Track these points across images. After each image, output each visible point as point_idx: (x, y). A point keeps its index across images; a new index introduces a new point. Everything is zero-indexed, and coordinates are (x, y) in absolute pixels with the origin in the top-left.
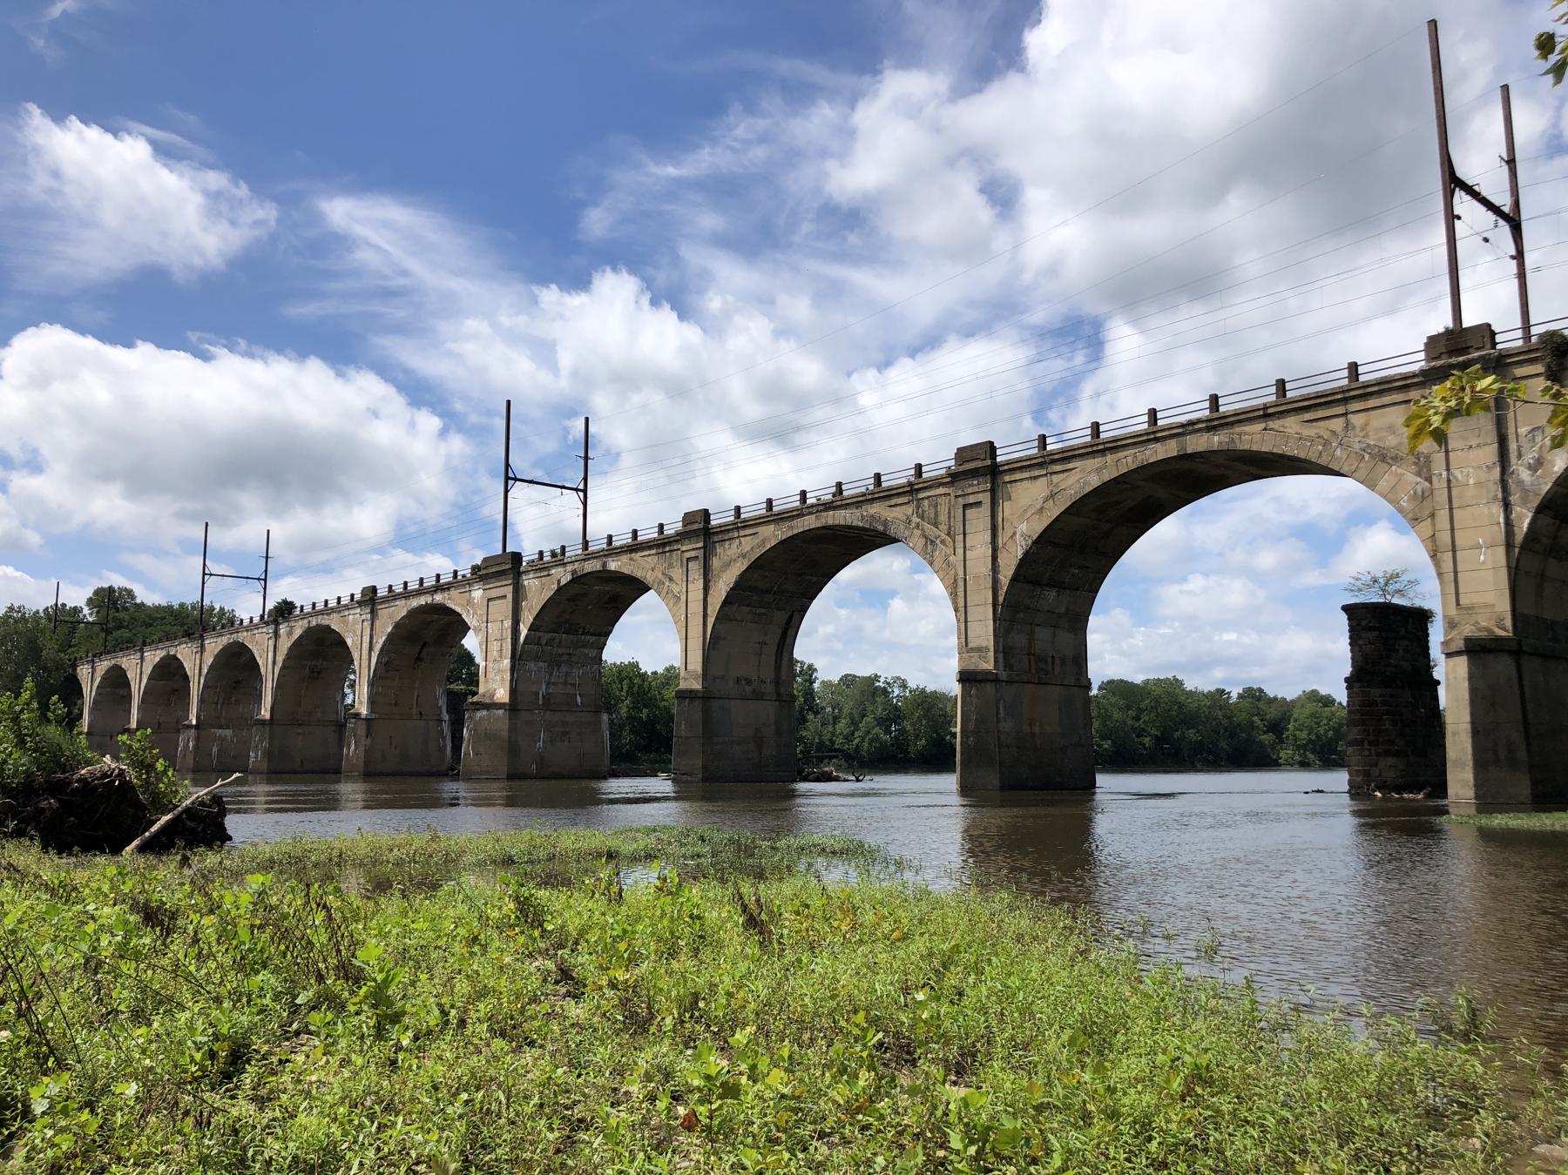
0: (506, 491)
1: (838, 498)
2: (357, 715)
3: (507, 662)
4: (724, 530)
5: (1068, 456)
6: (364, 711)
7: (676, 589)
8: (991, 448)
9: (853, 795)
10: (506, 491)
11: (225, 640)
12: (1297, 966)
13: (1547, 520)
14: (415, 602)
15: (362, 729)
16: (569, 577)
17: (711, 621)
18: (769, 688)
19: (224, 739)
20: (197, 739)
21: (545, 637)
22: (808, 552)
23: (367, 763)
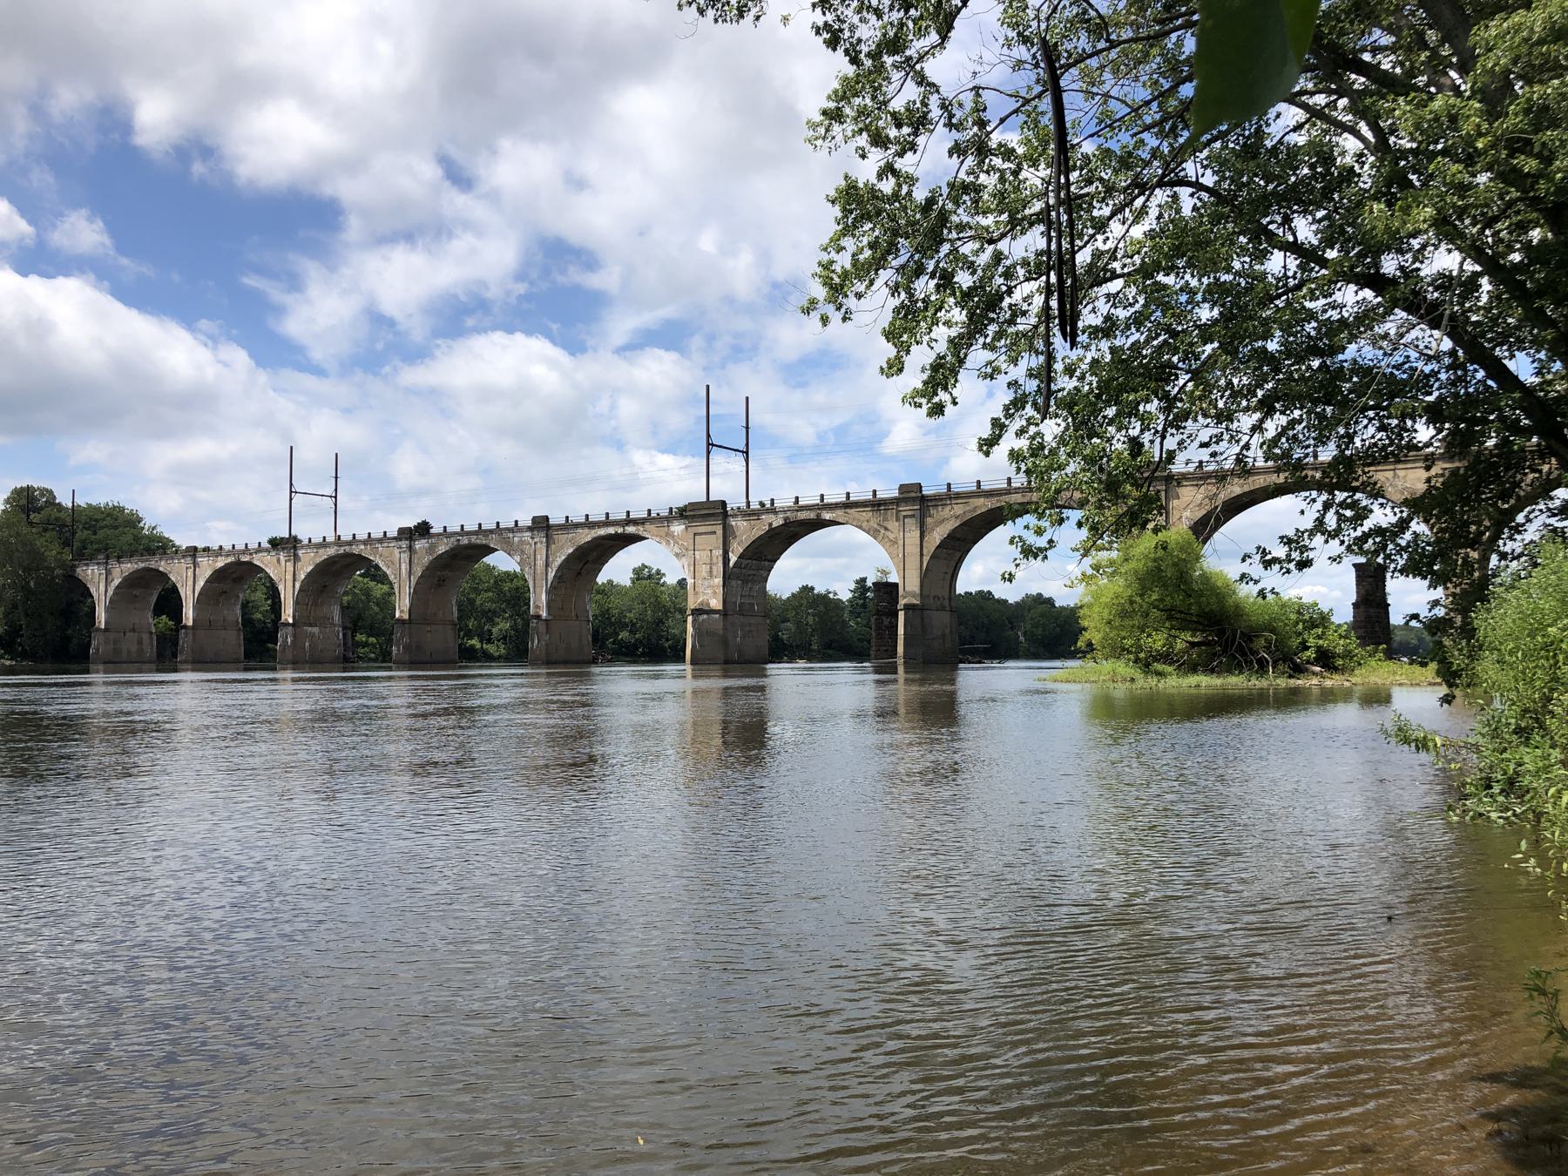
1: (480, 531)
2: (538, 617)
3: (719, 581)
4: (561, 527)
5: (577, 525)
6: (544, 614)
8: (547, 518)
9: (240, 681)
11: (129, 567)
12: (377, 750)
14: (602, 532)
15: (542, 628)
17: (926, 559)
18: (946, 603)
19: (312, 635)
20: (294, 636)
21: (745, 562)
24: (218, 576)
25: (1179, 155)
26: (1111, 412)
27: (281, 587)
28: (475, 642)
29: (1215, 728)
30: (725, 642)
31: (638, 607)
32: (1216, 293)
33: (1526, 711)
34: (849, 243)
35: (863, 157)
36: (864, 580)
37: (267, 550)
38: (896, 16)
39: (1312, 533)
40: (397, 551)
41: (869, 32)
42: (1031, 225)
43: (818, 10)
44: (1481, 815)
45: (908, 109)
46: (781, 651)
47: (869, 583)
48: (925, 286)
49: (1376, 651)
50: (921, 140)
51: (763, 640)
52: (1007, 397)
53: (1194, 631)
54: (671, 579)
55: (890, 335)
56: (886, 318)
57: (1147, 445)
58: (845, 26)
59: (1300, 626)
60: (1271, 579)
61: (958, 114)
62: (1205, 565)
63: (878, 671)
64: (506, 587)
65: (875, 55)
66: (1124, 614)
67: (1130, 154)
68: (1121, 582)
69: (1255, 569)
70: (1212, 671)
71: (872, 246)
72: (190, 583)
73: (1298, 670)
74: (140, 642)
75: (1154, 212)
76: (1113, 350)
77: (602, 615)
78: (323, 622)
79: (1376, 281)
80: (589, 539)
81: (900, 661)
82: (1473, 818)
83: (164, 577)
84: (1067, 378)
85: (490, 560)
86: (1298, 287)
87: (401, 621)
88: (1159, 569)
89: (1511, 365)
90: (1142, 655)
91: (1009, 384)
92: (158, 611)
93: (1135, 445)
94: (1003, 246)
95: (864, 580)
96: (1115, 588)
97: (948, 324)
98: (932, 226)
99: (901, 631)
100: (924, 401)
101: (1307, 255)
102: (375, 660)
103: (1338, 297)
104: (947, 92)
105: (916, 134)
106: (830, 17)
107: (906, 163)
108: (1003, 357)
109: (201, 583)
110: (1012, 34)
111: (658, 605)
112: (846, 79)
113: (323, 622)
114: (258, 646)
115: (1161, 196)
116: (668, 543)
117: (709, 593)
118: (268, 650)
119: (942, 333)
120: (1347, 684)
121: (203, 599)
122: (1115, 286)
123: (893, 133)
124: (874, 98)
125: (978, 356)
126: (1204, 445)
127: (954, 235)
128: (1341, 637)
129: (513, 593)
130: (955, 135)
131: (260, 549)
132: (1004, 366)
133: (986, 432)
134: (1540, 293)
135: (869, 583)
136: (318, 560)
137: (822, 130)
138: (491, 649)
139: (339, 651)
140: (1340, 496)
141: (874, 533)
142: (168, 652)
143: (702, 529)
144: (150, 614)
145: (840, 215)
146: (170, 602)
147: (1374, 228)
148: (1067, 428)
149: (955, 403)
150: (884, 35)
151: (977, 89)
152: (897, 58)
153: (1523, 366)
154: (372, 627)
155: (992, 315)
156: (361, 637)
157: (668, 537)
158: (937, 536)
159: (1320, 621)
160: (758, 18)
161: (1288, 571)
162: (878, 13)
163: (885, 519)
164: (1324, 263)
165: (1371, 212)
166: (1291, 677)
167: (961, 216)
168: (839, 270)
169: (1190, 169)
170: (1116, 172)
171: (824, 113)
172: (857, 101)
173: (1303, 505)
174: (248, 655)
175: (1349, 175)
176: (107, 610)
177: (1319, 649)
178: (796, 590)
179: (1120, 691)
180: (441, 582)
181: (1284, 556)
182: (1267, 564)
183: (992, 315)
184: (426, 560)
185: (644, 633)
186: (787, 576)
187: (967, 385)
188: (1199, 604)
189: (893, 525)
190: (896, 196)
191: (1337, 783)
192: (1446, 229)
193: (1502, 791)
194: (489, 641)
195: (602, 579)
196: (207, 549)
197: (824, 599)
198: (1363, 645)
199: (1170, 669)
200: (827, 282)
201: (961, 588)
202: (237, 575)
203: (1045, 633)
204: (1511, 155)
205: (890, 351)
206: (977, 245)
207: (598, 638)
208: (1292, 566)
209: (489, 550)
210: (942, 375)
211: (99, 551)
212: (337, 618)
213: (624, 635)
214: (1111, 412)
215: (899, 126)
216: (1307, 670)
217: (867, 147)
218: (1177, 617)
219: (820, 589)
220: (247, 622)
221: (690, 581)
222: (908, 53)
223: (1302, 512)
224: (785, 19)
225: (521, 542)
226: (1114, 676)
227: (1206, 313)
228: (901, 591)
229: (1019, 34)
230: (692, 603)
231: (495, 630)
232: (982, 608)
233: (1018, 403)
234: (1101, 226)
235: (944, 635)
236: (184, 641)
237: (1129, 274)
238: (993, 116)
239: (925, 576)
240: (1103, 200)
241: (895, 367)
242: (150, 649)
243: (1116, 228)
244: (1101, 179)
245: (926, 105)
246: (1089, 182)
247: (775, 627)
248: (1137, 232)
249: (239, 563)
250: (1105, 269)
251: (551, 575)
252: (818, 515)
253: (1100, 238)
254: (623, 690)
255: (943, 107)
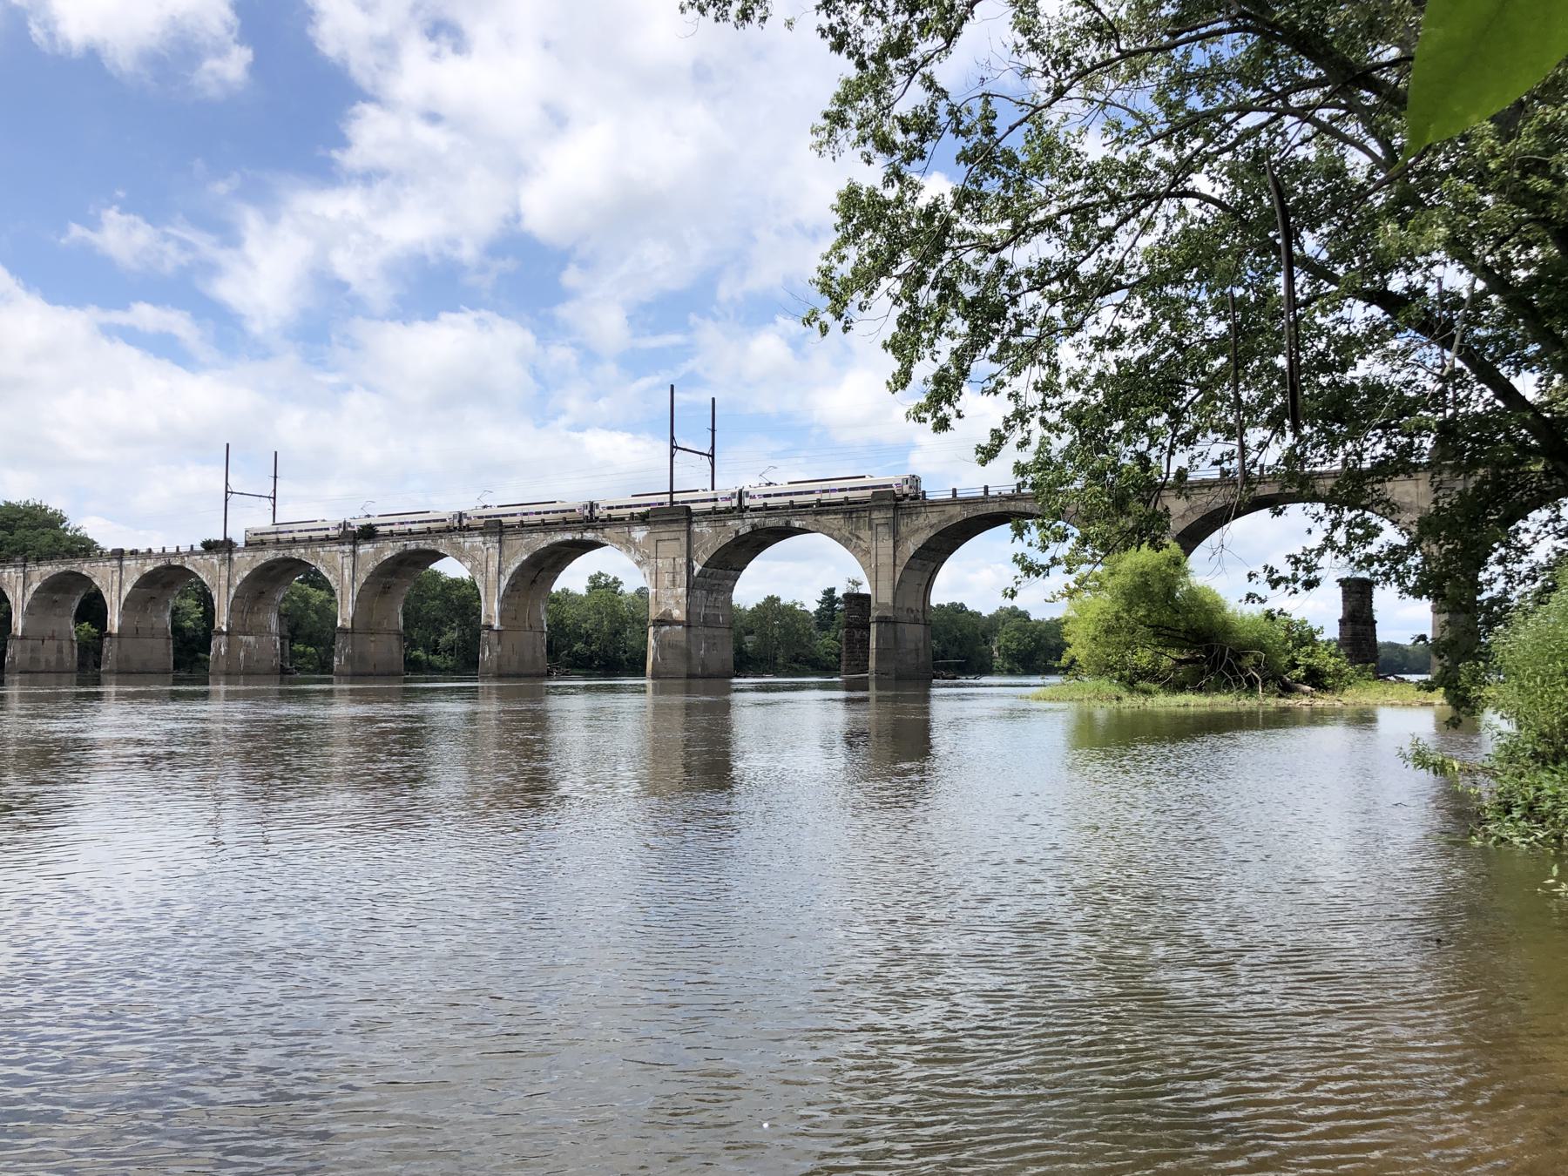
0: (672, 456)
2: (490, 627)
3: (682, 590)
6: (496, 624)
7: (864, 545)
10: (672, 456)
13: (92, 590)
15: (494, 637)
16: (748, 529)
17: (900, 569)
18: (920, 616)
19: (248, 645)
20: (228, 645)
21: (710, 571)
22: (582, 529)
23: (499, 666)
24: (147, 580)
25: (1189, 166)
26: (1118, 426)
27: (214, 593)
28: (420, 653)
29: (1198, 751)
30: (688, 656)
31: (594, 618)
32: (1224, 307)
33: (1542, 735)
34: (852, 252)
35: (869, 162)
36: (832, 590)
37: (199, 553)
38: (902, 18)
39: (1320, 552)
40: (339, 556)
41: (873, 36)
42: (1036, 232)
43: (823, 13)
44: (1503, 840)
45: (915, 115)
46: (746, 663)
47: (839, 594)
48: (927, 296)
49: (1365, 670)
50: (928, 146)
51: (727, 654)
52: (1009, 408)
53: (1181, 648)
54: (629, 587)
55: (895, 346)
56: (891, 328)
57: (1154, 460)
58: (850, 29)
59: (1290, 644)
60: (1279, 600)
61: (967, 121)
62: (1192, 579)
63: (849, 687)
64: (455, 594)
65: (879, 59)
66: (1109, 631)
67: (1136, 165)
68: (1106, 596)
69: (1263, 589)
70: (1200, 689)
71: (872, 255)
72: (115, 589)
73: (1287, 690)
74: (60, 650)
75: (1161, 225)
76: (1119, 364)
77: (556, 626)
78: (261, 631)
79: (1380, 297)
80: (544, 545)
81: (871, 674)
82: (1496, 843)
83: (87, 581)
84: (1073, 391)
85: (436, 566)
86: (1307, 303)
87: (343, 630)
88: (1146, 583)
89: (1516, 382)
90: (1127, 673)
91: (1010, 395)
92: (80, 617)
93: (1142, 459)
94: (1006, 254)
95: (832, 590)
96: (1100, 603)
97: (952, 335)
98: (934, 234)
99: (873, 644)
100: (928, 416)
101: (1318, 271)
102: (314, 672)
103: (1346, 313)
104: (956, 99)
105: (922, 140)
106: (835, 19)
107: (912, 171)
108: (1006, 371)
109: (128, 588)
110: (1022, 40)
111: (614, 615)
112: (848, 82)
113: (261, 631)
114: (188, 659)
115: (1170, 207)
116: (629, 551)
117: (673, 602)
118: (198, 660)
119: (945, 346)
120: (1338, 704)
121: (130, 604)
122: (1119, 296)
123: (899, 137)
124: (877, 102)
125: (982, 366)
126: (1215, 463)
127: (956, 243)
128: (1331, 655)
129: (462, 600)
130: (961, 140)
131: (192, 552)
132: (1007, 379)
133: (986, 441)
134: (1549, 312)
135: (839, 594)
136: (255, 565)
137: (825, 135)
138: (436, 660)
139: (276, 661)
140: (1348, 515)
141: (845, 542)
142: (91, 662)
143: (665, 536)
144: (71, 621)
145: (839, 221)
146: (93, 609)
147: (1388, 248)
148: (1073, 443)
149: (959, 416)
150: (888, 38)
151: (986, 97)
152: (901, 61)
153: (1527, 384)
154: (310, 636)
155: (995, 325)
156: (299, 647)
157: (628, 544)
158: (911, 546)
159: (1305, 638)
160: (764, 19)
161: (1295, 592)
162: (882, 16)
163: (858, 528)
164: (1333, 279)
165: (1386, 230)
166: (1280, 696)
167: (964, 225)
168: (838, 277)
169: (1200, 182)
170: (1122, 181)
171: (826, 116)
172: (861, 104)
173: (1310, 523)
174: (177, 665)
175: (1362, 193)
176: (24, 615)
177: (1308, 667)
178: (761, 600)
179: (1102, 712)
180: (386, 589)
181: (1260, 567)
182: (1275, 584)
183: (995, 325)
184: (371, 567)
185: (599, 648)
186: (753, 586)
187: (969, 399)
188: (1186, 620)
189: (865, 534)
190: (900, 202)
191: (1335, 813)
192: (1459, 250)
193: (1523, 816)
194: (435, 652)
195: (557, 587)
196: (134, 553)
197: (790, 611)
198: (1352, 664)
199: (1154, 687)
200: (826, 289)
201: (934, 603)
202: (166, 579)
203: (1035, 651)
204: (1524, 176)
205: (893, 364)
206: (980, 254)
207: (552, 651)
208: (1298, 586)
209: (438, 556)
210: (946, 388)
211: (16, 552)
212: (274, 627)
213: (578, 646)
214: (1118, 426)
215: (906, 131)
216: (1297, 690)
217: (873, 152)
218: (1165, 634)
219: (786, 600)
220: (177, 630)
221: (652, 591)
222: (912, 56)
223: (1310, 531)
224: (789, 24)
225: (473, 548)
226: (1105, 700)
227: (1216, 327)
228: (873, 604)
229: (1030, 41)
230: (654, 614)
231: (442, 641)
232: (954, 622)
233: (1021, 416)
234: (1108, 236)
235: (917, 650)
236: (110, 650)
237: (1134, 285)
238: (1001, 125)
239: (897, 590)
240: (1109, 210)
241: (902, 380)
242: (71, 658)
243: (1123, 239)
244: (1106, 189)
245: (934, 112)
246: (1094, 191)
247: (738, 640)
248: (1145, 242)
249: (170, 567)
250: (1111, 281)
251: (504, 583)
252: (788, 523)
253: (1106, 248)
254: (574, 710)
255: (951, 113)
